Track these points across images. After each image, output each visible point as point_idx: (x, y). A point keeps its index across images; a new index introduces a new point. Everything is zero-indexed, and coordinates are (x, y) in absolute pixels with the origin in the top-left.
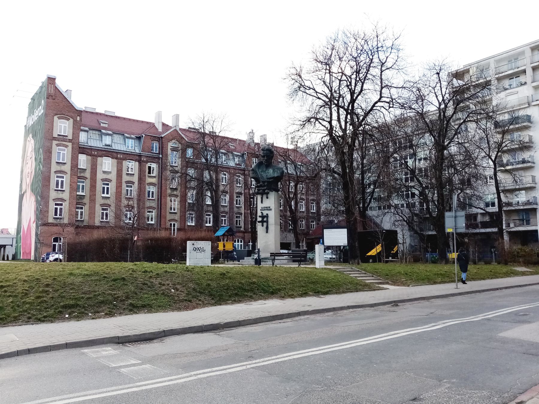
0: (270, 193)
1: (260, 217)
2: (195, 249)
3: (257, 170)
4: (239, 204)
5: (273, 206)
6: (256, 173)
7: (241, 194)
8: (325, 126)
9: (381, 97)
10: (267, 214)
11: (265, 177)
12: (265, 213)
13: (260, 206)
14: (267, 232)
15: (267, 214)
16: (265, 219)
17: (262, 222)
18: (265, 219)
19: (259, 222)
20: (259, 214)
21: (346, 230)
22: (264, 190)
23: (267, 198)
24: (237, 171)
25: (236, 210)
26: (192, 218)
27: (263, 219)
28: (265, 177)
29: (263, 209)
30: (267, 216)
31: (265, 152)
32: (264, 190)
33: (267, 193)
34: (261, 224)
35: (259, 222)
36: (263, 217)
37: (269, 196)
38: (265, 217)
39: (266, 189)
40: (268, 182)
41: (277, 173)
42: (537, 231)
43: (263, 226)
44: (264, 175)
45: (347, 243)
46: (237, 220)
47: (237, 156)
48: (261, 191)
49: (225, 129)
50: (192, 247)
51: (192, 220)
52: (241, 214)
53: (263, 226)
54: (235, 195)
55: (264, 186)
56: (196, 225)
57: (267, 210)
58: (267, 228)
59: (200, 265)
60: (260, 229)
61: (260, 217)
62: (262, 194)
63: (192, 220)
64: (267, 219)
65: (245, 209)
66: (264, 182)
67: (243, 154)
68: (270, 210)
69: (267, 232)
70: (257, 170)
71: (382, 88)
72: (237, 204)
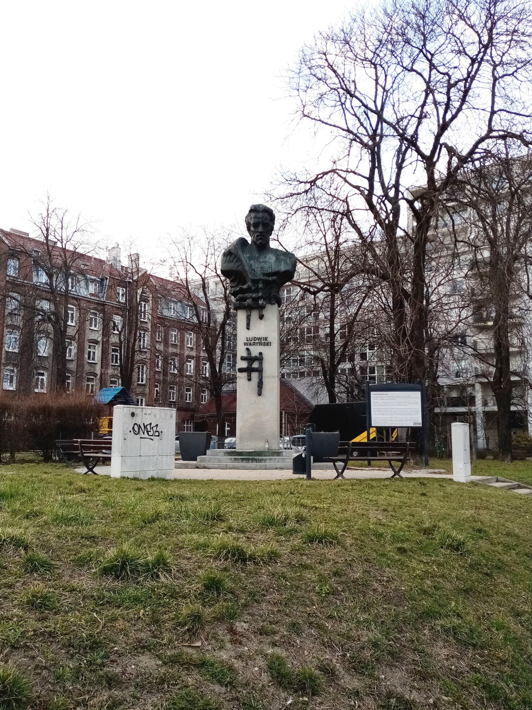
0: (269, 306)
1: (243, 358)
2: (138, 429)
3: (240, 253)
4: (93, 359)
5: (274, 337)
6: (239, 260)
7: (96, 342)
8: (358, 188)
9: (490, 130)
10: (261, 354)
11: (258, 271)
12: (255, 351)
13: (243, 334)
14: (260, 394)
15: (261, 354)
16: (254, 365)
17: (249, 370)
18: (256, 365)
19: (241, 370)
20: (241, 351)
21: (418, 394)
22: (256, 300)
23: (261, 317)
24: (92, 306)
25: (87, 368)
26: (12, 377)
27: (250, 364)
28: (258, 271)
29: (250, 342)
30: (260, 358)
31: (260, 215)
32: (256, 300)
33: (261, 308)
34: (245, 375)
35: (241, 370)
36: (250, 359)
37: (265, 312)
38: (256, 359)
39: (260, 298)
40: (265, 282)
41: (286, 263)
42: (526, 412)
43: (249, 380)
44: (256, 266)
45: (420, 421)
46: (88, 385)
47: (93, 281)
48: (249, 301)
49: (83, 228)
50: (130, 422)
51: (11, 382)
52: (95, 375)
53: (249, 380)
54: (87, 344)
55: (257, 290)
56: (18, 389)
57: (261, 344)
58: (260, 385)
59: (149, 475)
60: (244, 387)
61: (243, 358)
62: (249, 309)
63: (11, 382)
64: (261, 364)
65: (102, 367)
66: (255, 282)
67: (102, 280)
68: (268, 344)
69: (260, 394)
70: (240, 253)
71: (493, 113)
72: (89, 358)
